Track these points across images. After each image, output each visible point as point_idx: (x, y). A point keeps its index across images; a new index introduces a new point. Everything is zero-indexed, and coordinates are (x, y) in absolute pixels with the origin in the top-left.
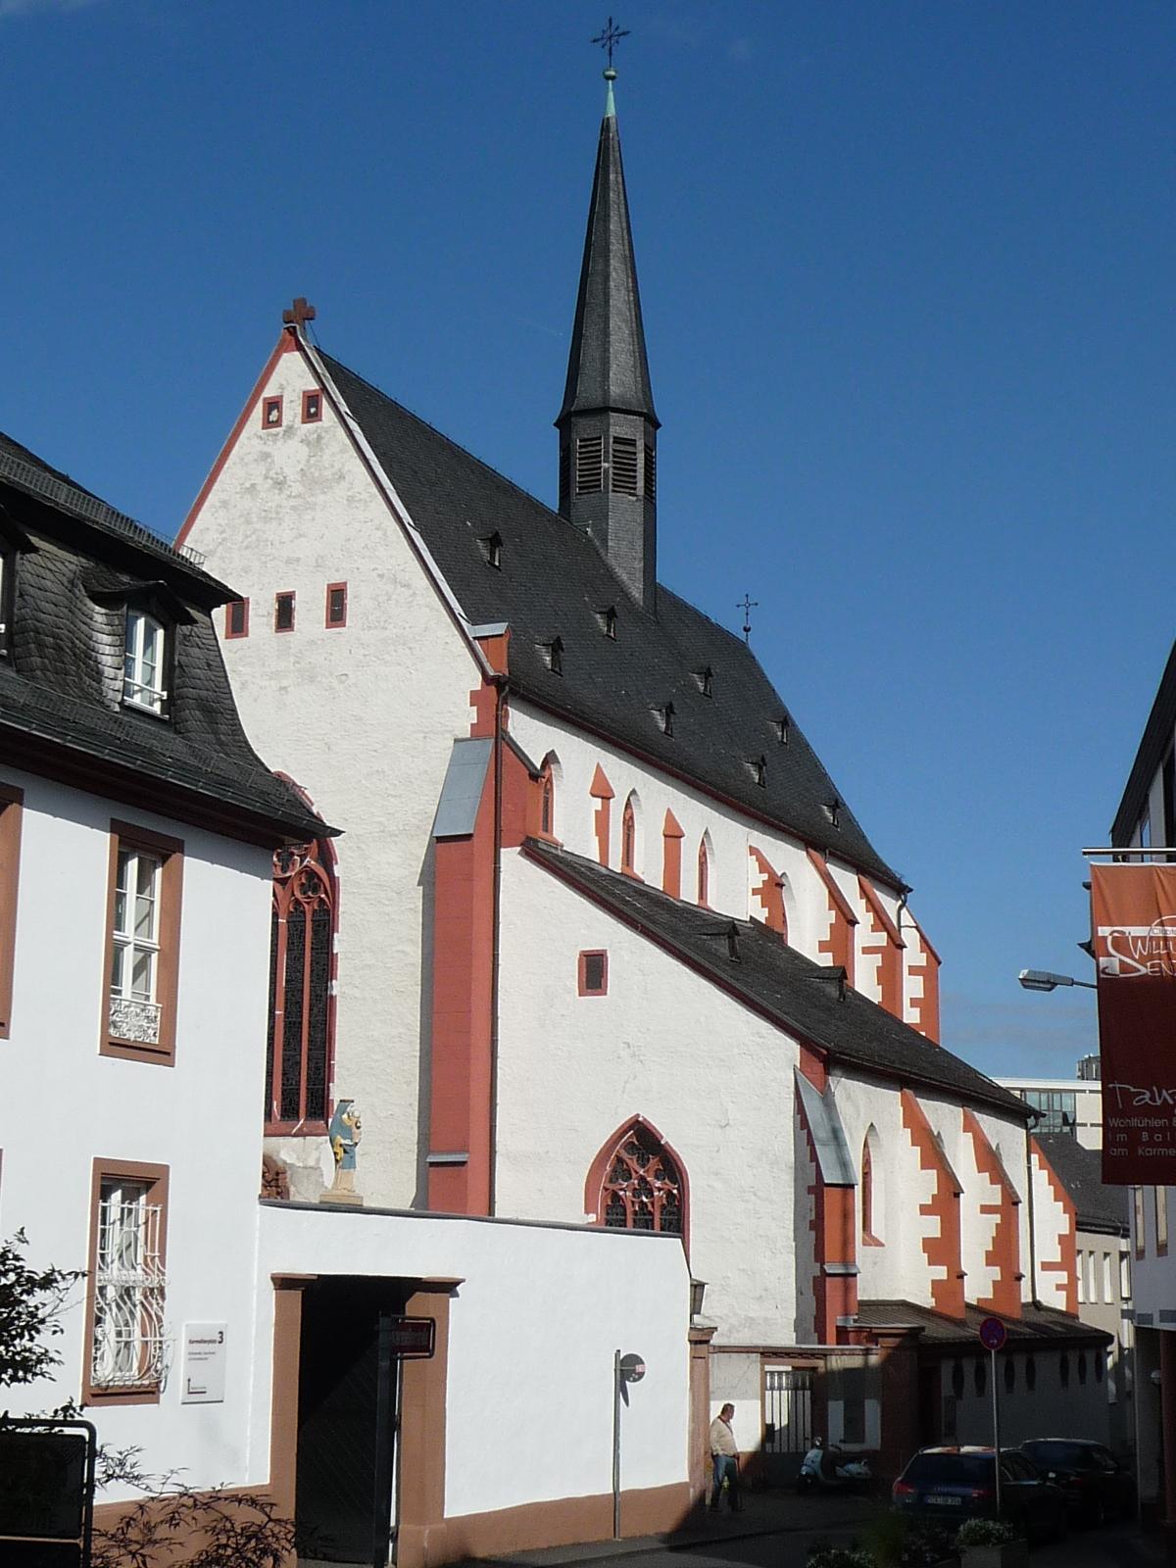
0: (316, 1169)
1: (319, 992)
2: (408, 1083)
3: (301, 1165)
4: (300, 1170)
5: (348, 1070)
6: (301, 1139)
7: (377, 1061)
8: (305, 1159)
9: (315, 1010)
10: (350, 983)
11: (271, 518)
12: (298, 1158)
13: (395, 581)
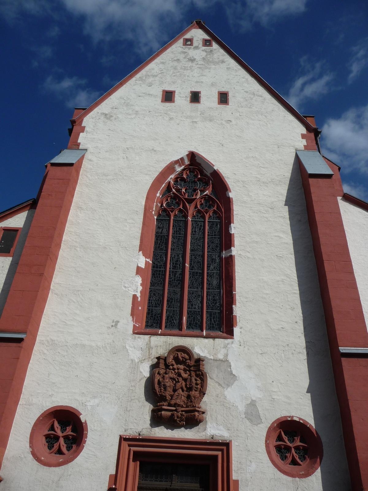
0: (224, 361)
1: (214, 257)
2: (293, 309)
3: (212, 357)
4: (211, 361)
5: (246, 298)
6: (211, 340)
7: (267, 294)
8: (215, 354)
9: (212, 267)
10: (243, 250)
11: (187, 69)
12: (209, 353)
13: (254, 94)
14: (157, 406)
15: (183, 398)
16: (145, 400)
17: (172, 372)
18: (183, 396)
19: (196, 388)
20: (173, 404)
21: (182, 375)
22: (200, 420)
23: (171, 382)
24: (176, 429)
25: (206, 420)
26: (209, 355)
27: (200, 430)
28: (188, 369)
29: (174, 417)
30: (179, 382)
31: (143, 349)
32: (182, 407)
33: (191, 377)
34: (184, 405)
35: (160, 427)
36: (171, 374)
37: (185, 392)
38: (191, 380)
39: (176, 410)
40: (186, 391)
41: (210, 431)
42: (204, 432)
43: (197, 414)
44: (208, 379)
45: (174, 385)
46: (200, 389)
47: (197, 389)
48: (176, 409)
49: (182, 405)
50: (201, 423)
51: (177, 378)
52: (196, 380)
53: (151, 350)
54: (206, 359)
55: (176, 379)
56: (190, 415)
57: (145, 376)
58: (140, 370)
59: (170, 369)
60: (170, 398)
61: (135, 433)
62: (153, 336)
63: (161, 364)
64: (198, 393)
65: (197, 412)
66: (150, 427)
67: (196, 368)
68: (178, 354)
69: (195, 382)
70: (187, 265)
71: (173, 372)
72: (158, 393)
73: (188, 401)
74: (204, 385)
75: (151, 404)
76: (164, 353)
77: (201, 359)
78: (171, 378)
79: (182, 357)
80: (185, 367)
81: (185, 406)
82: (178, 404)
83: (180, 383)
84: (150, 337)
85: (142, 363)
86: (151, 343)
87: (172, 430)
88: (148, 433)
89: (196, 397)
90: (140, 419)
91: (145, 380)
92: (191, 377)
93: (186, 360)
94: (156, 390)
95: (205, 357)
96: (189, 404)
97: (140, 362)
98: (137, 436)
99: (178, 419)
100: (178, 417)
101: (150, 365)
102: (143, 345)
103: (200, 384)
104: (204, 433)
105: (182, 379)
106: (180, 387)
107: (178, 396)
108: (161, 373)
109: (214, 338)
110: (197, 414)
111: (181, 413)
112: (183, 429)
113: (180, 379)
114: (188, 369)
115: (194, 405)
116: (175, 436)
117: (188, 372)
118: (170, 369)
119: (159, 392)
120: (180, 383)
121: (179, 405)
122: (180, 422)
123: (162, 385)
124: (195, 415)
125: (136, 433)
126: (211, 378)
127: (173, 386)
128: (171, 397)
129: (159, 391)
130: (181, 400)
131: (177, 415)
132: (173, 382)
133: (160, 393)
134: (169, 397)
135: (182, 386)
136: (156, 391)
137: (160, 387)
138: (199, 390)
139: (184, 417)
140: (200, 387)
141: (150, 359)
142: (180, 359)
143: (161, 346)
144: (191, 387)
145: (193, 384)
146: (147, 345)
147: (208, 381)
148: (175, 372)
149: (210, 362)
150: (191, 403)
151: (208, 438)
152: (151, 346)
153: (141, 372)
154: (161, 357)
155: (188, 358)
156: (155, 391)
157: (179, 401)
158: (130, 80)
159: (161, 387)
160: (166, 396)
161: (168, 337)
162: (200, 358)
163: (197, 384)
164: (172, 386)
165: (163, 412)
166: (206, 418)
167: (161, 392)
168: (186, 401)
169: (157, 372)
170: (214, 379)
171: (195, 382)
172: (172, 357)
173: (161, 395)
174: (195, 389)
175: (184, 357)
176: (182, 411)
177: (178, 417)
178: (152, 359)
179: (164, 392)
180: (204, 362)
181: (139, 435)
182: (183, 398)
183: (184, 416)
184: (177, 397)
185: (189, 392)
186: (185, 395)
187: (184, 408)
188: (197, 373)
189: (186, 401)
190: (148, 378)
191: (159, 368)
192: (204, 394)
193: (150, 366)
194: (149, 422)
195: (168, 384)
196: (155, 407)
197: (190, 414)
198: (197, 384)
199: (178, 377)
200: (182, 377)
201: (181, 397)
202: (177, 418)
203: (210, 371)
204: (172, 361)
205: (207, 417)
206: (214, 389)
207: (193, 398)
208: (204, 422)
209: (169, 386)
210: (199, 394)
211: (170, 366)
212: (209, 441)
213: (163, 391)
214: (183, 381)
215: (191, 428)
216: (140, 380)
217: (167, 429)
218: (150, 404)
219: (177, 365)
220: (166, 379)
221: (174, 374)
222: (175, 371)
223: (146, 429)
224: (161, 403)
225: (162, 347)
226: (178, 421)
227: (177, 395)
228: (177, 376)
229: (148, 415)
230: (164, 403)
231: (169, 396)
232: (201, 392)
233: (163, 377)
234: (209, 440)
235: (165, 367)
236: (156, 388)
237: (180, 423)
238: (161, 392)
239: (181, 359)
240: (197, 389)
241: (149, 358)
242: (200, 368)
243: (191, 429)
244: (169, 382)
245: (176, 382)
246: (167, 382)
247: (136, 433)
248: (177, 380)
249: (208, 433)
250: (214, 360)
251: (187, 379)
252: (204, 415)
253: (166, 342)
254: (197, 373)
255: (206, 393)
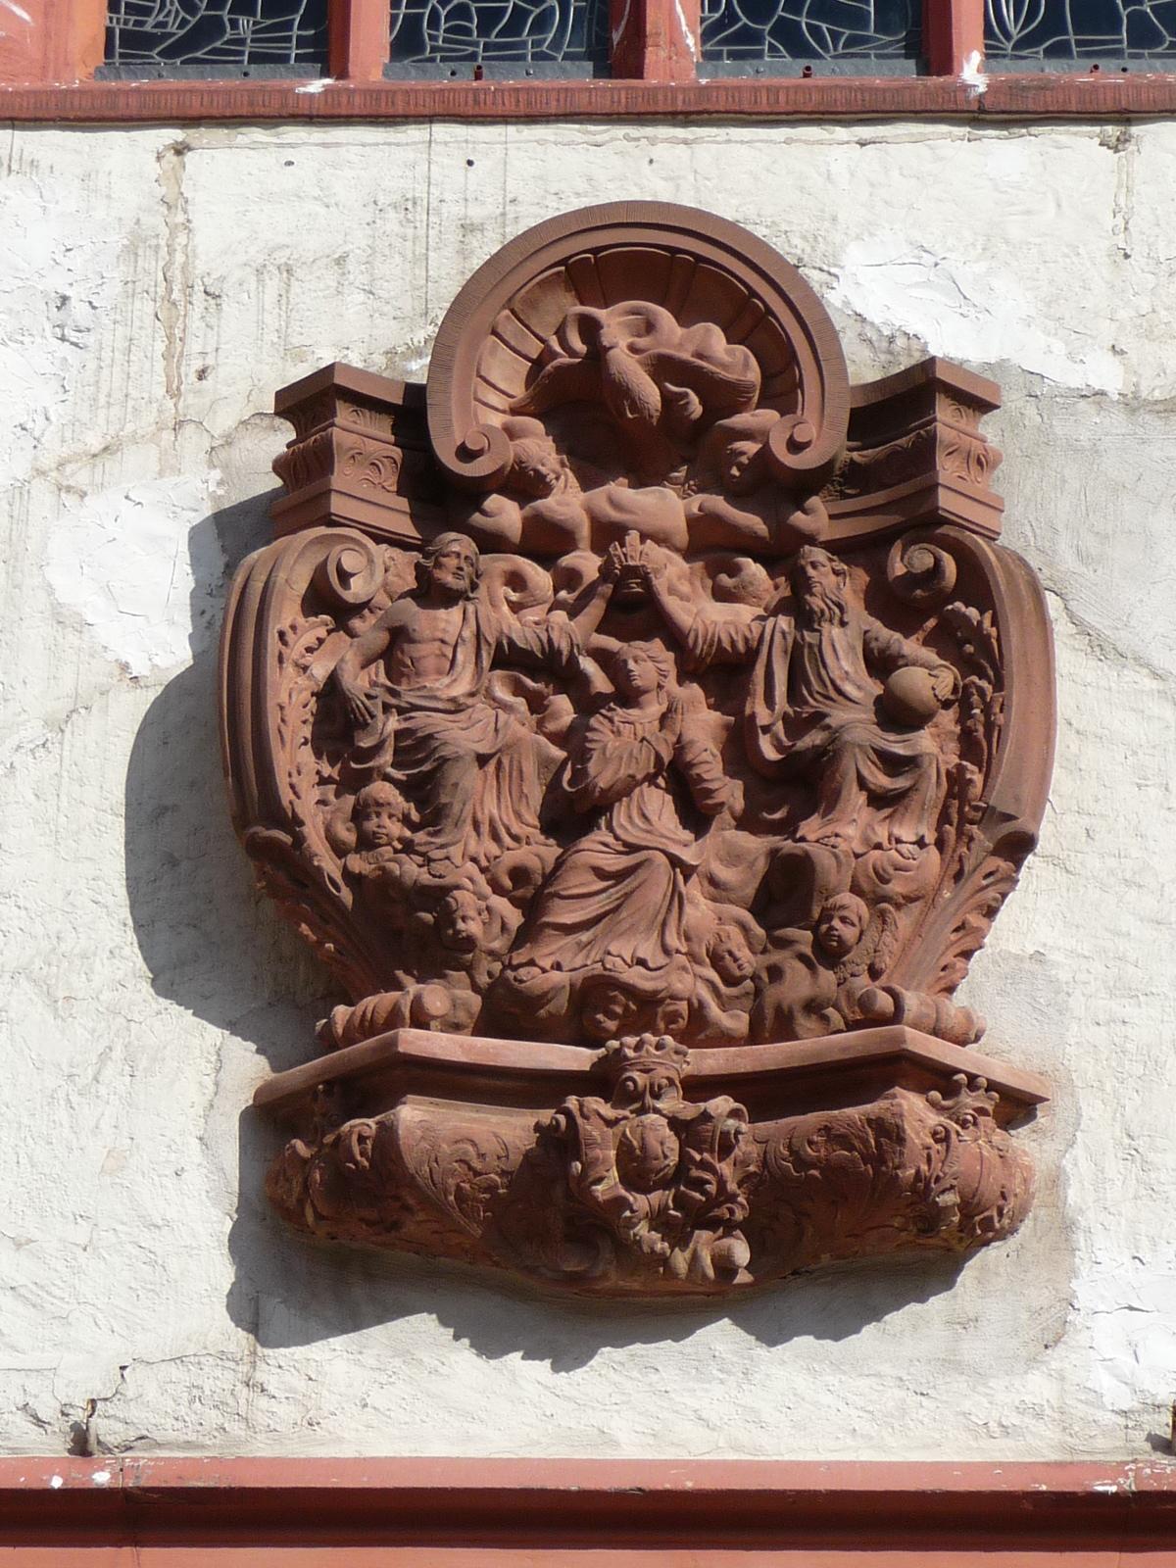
3: (1109, 376)
14: (329, 1042)
15: (700, 909)
16: (146, 988)
17: (516, 580)
18: (694, 889)
19: (893, 764)
20: (557, 989)
21: (672, 604)
22: (970, 1207)
23: (507, 708)
24: (619, 1342)
25: (1057, 1203)
26: (1059, 347)
27: (972, 1348)
28: (753, 522)
29: (577, 1166)
30: (627, 695)
31: (79, 311)
32: (696, 1029)
33: (805, 618)
34: (724, 1007)
35: (376, 1332)
36: (516, 607)
37: (726, 834)
38: (802, 664)
39: (605, 1081)
40: (747, 822)
41: (1125, 1360)
42: (1033, 1361)
43: (915, 1110)
44: (1069, 658)
45: (559, 754)
46: (957, 782)
47: (901, 783)
48: (602, 1061)
49: (698, 1012)
50: (992, 1255)
51: (603, 657)
52: (881, 663)
53: (195, 323)
54: (1012, 400)
55: (588, 665)
56: (826, 1130)
57: (125, 667)
58: (50, 590)
59: (491, 542)
60: (515, 918)
61: (23, 1423)
62: (221, 134)
63: (345, 476)
64: (930, 838)
65: (922, 1089)
66: (239, 1339)
67: (878, 498)
68: (590, 328)
69: (876, 689)
70: (646, 1299)
71: (540, 578)
72: (329, 865)
73: (783, 944)
74: (1015, 722)
75: (234, 1027)
76: (391, 353)
77: (941, 374)
78: (508, 657)
79: (664, 368)
80: (718, 503)
81: (736, 1021)
82: (629, 990)
83: (654, 708)
84: (180, 150)
85: (70, 500)
86: (187, 226)
87: (566, 1359)
88: (213, 1418)
89: (895, 887)
90: (81, 1233)
91: (130, 710)
92: (805, 618)
93: (723, 396)
94: (293, 823)
95: (1002, 365)
96: (799, 983)
97: (42, 494)
98: (49, 1465)
99: (641, 1202)
100: (636, 1169)
101: (197, 518)
102: (76, 260)
103: (947, 719)
104: (1037, 1386)
105: (668, 659)
106: (645, 765)
107: (620, 876)
108: (357, 590)
109: (1125, 117)
110: (915, 1110)
111: (688, 1110)
112: (721, 1337)
113: (650, 661)
114: (753, 522)
115: (865, 1003)
116: (615, 1444)
117: (754, 569)
118: (491, 542)
119: (339, 849)
120: (654, 708)
121: (645, 1011)
122: (678, 1235)
123: (378, 748)
124: (890, 1132)
125: (39, 1422)
126: (1099, 646)
127: (545, 762)
128: (516, 902)
129: (349, 837)
130: (673, 940)
131: (625, 1150)
132: (537, 704)
133: (357, 863)
134: (501, 904)
135: (680, 747)
136: (299, 840)
137: (352, 782)
138: (933, 791)
139: (725, 1168)
140: (953, 746)
141: (193, 443)
142: (623, 392)
143: (340, 261)
144: (819, 752)
145: (838, 716)
146: (131, 251)
147: (1066, 698)
148: (568, 579)
149: (1084, 437)
150: (827, 977)
151: (1101, 1443)
152: (200, 267)
153: (63, 618)
154: (338, 380)
155: (754, 375)
156: (285, 838)
157: (648, 949)
158: (277, 788)
159: (366, 777)
160: (446, 890)
161: (441, 131)
162: (930, 364)
163: (897, 714)
164: (530, 767)
165: (412, 1114)
166: (1056, 1181)
167: (367, 842)
168: (744, 954)
169: (302, 586)
170: (1140, 661)
171: (876, 689)
172: (508, 375)
173: (379, 890)
174: (881, 780)
175: (684, 365)
176: (698, 1087)
177: (636, 1169)
178: (229, 441)
179: (420, 837)
180: (989, 428)
181: (82, 1444)
182: (700, 909)
183: (726, 1146)
184: (616, 892)
185: (787, 828)
186: (725, 874)
187: (726, 1039)
188: (898, 568)
189: (744, 954)
190: (177, 691)
191: (330, 521)
192: (1018, 846)
193: (195, 534)
194: (223, 1273)
195: (464, 736)
196: (279, 1072)
197: (814, 1118)
198: (897, 714)
199: (612, 643)
200: (674, 637)
201: (677, 898)
202: (627, 1180)
203: (1081, 556)
204: (511, 432)
205: (1079, 1168)
206: (1153, 792)
207: (846, 898)
208: (1025, 1229)
209: (482, 760)
210: (940, 844)
211: (494, 501)
212: (1129, 1485)
213: (396, 829)
214: (695, 690)
215: (837, 1328)
216: (59, 725)
217: (490, 1345)
218: (215, 1034)
219: (587, 484)
220: (429, 663)
221: (557, 605)
222: (566, 561)
223: (175, 1372)
224: (377, 1003)
225: (357, 274)
226: (642, 1230)
227: (614, 863)
228: (600, 629)
229: (197, 1179)
230: (413, 987)
231: (498, 889)
232: (963, 819)
233: (397, 642)
234: (1119, 1468)
235: (414, 517)
236: (286, 795)
237: (680, 1260)
238: (367, 842)
239: (650, 394)
240: (901, 783)
241: (178, 426)
242: (933, 487)
243: (837, 1338)
244: (482, 710)
245: (588, 704)
246: (456, 707)
247: (39, 1422)
248: (601, 683)
249: (1104, 1382)
250: (1133, 404)
251: (752, 653)
252: (1021, 1139)
253: (406, 205)
254: (898, 568)
255: (1046, 834)
